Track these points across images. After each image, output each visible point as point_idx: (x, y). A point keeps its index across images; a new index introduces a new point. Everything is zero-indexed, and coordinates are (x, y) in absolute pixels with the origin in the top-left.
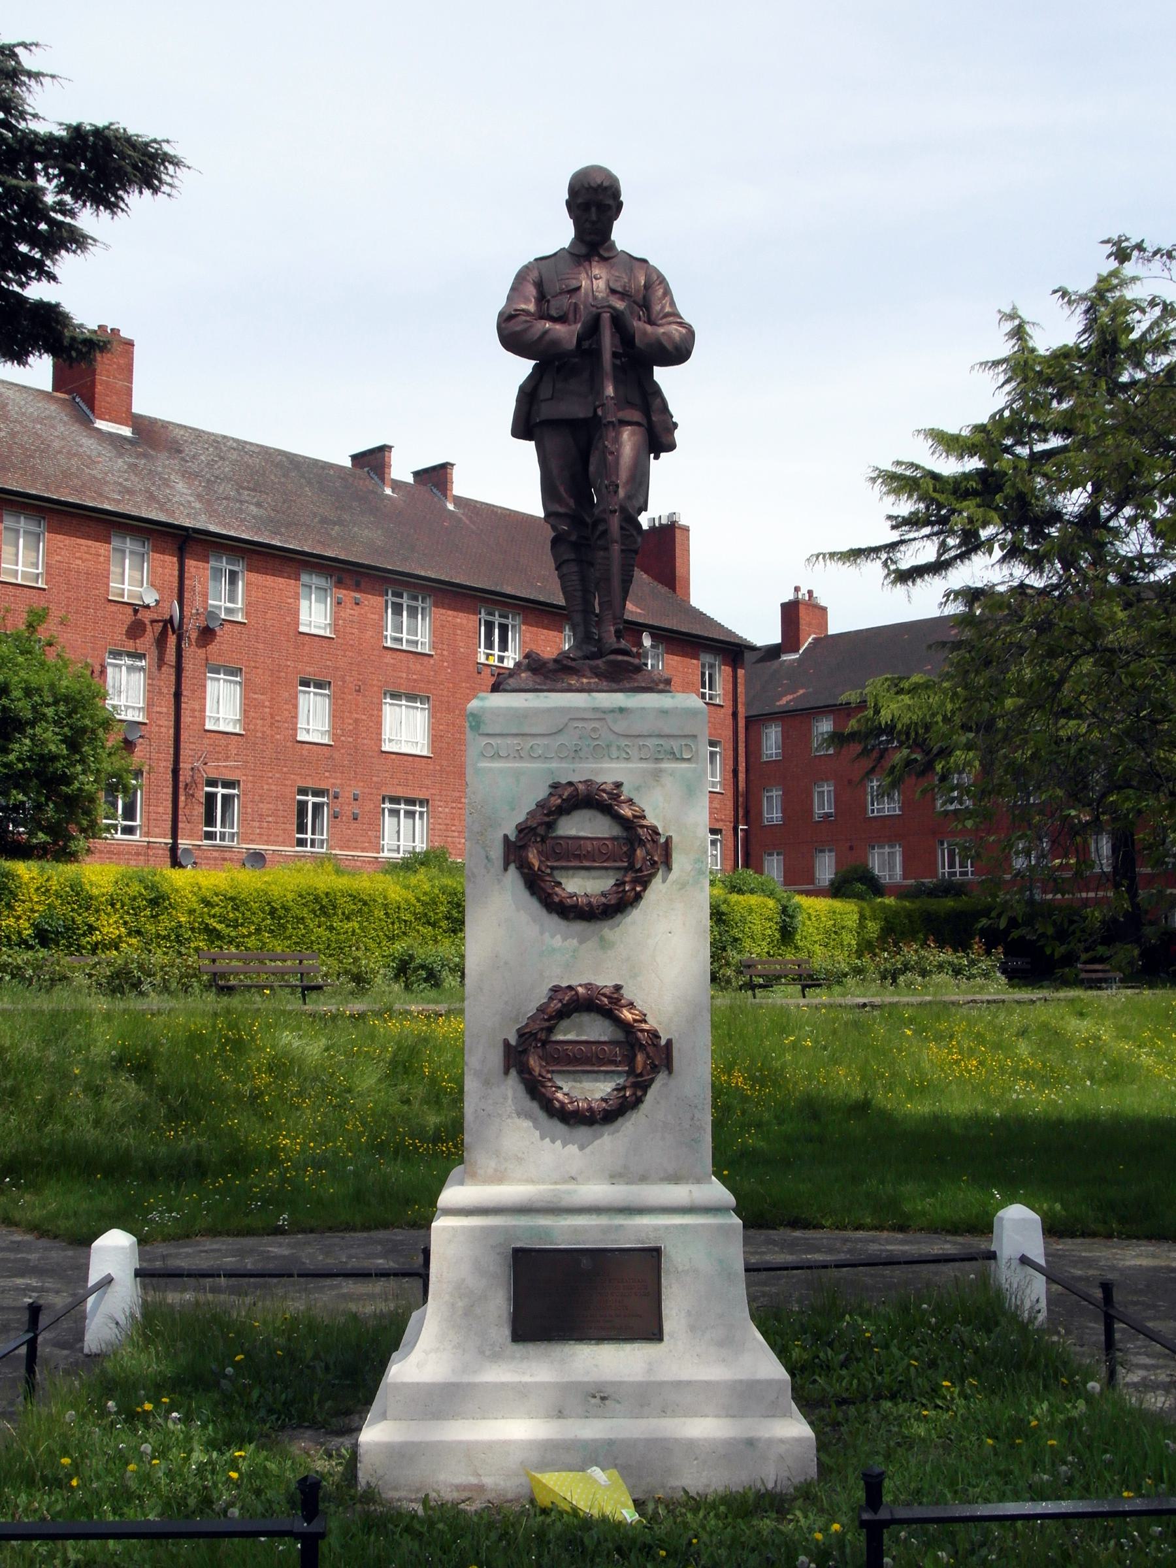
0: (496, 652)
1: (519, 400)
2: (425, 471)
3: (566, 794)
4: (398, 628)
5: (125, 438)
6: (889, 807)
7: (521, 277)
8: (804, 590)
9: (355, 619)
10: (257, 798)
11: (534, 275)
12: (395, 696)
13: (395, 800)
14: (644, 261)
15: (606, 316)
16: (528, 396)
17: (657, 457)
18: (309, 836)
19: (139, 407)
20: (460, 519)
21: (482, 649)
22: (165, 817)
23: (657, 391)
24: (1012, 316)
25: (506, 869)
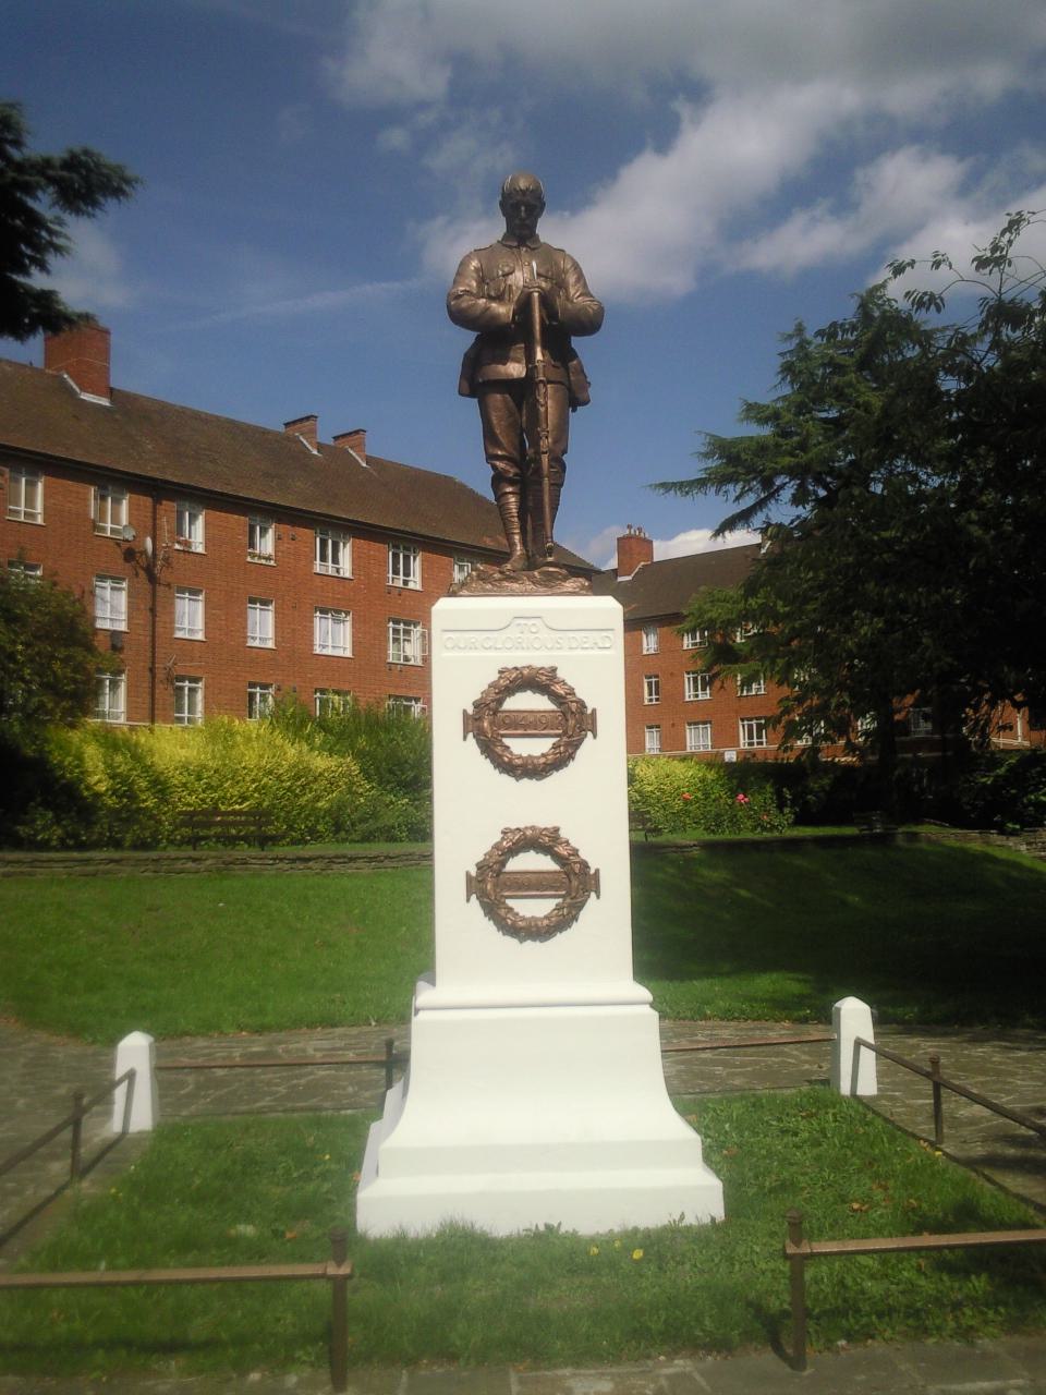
0: (401, 577)
3: (513, 676)
9: (292, 552)
10: (216, 691)
12: (324, 611)
14: (563, 251)
17: (574, 411)
19: (117, 381)
20: (371, 474)
21: (391, 575)
22: (145, 706)
25: (465, 738)
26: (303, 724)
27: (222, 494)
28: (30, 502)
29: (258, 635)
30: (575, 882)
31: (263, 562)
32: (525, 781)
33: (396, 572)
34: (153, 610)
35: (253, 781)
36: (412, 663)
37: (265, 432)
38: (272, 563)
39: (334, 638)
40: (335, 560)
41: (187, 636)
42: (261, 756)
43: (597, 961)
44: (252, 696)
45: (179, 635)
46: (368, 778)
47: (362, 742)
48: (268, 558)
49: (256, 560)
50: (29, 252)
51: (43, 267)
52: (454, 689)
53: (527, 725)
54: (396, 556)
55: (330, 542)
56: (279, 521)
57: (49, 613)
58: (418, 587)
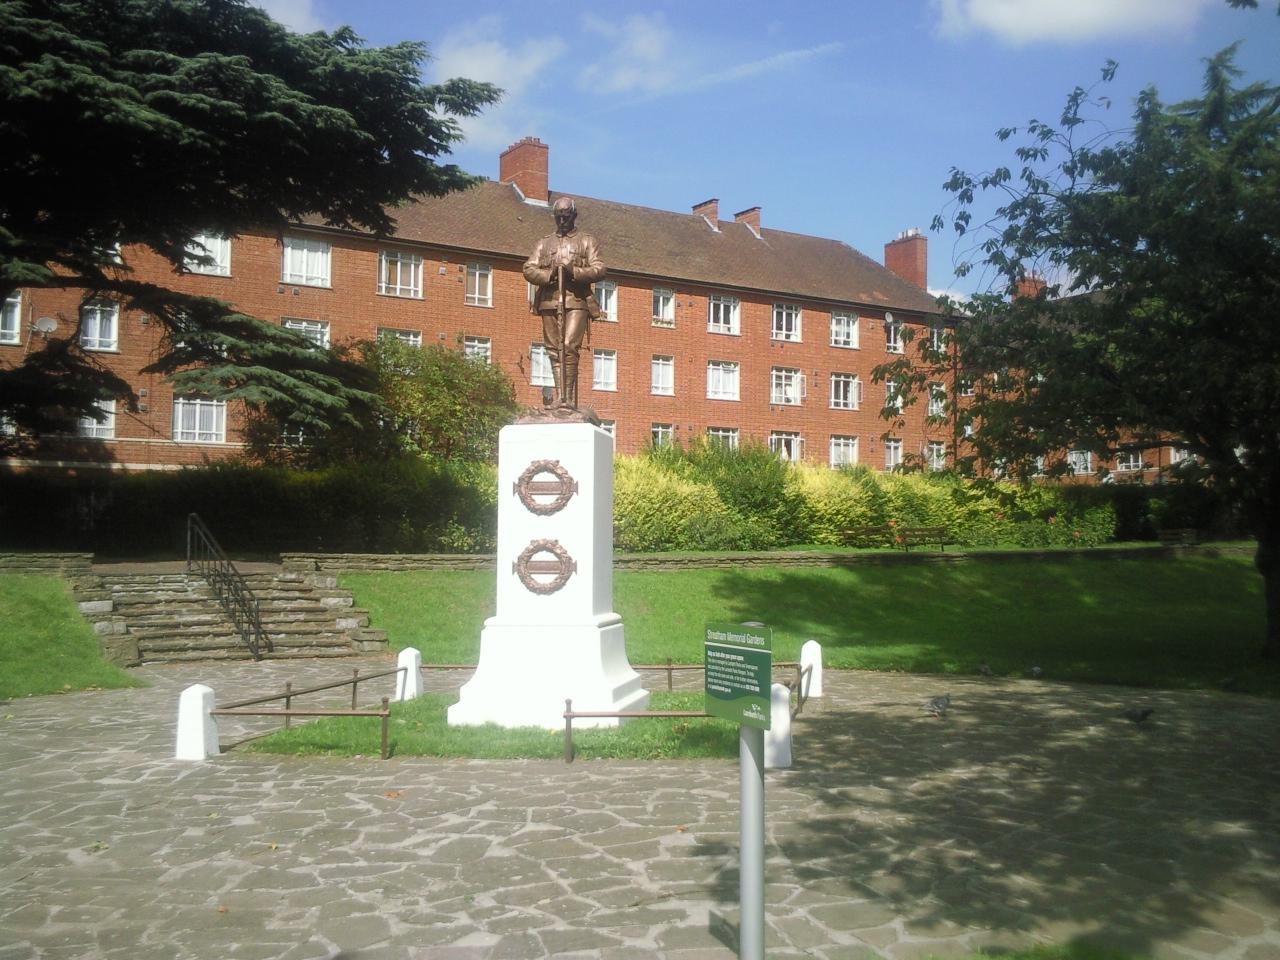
0: (784, 332)
4: (391, 280)
5: (542, 208)
13: (838, 437)
20: (764, 245)
21: (774, 331)
24: (1111, 63)
26: (676, 459)
27: (632, 273)
28: (483, 291)
29: (660, 385)
30: (565, 568)
31: (665, 325)
32: (542, 516)
33: (779, 328)
35: (631, 503)
36: (792, 403)
37: (675, 216)
38: (672, 326)
39: (724, 385)
40: (727, 321)
41: (603, 388)
42: (638, 485)
44: (655, 434)
45: (596, 387)
46: (725, 500)
47: (722, 473)
48: (670, 323)
49: (659, 325)
50: (435, 141)
51: (446, 150)
53: (544, 489)
54: (779, 315)
55: (722, 306)
56: (679, 292)
57: (479, 382)
58: (799, 340)
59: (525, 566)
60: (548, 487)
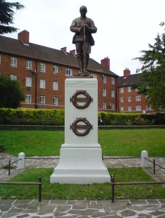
1: (73, 38)
2: (71, 51)
5: (28, 46)
6: (139, 100)
7: (73, 21)
8: (127, 68)
11: (75, 21)
15: (84, 27)
16: (74, 38)
18: (55, 103)
23: (92, 37)
30: (89, 127)
34: (36, 83)
43: (92, 141)
48: (57, 74)
52: (69, 93)
53: (81, 100)
59: (75, 127)
60: (81, 100)
